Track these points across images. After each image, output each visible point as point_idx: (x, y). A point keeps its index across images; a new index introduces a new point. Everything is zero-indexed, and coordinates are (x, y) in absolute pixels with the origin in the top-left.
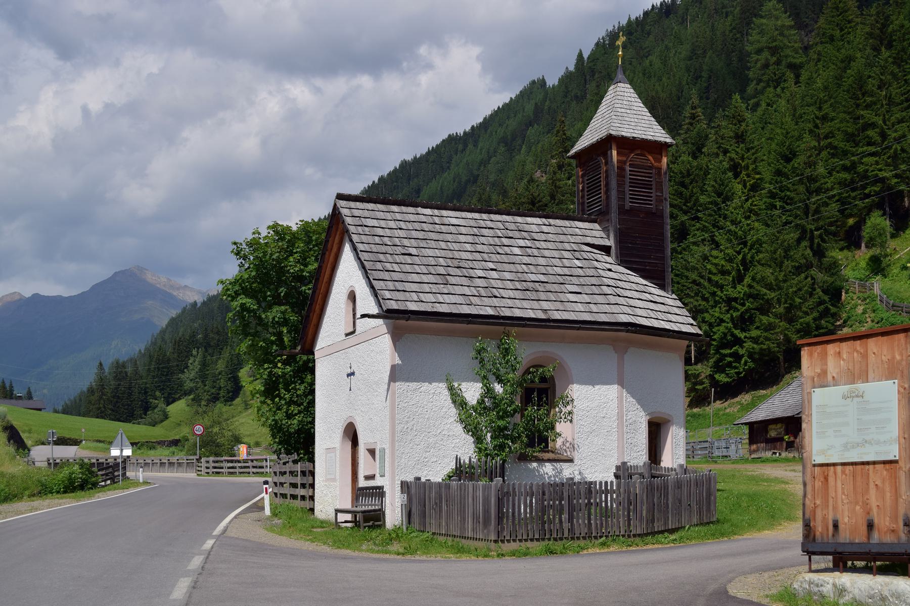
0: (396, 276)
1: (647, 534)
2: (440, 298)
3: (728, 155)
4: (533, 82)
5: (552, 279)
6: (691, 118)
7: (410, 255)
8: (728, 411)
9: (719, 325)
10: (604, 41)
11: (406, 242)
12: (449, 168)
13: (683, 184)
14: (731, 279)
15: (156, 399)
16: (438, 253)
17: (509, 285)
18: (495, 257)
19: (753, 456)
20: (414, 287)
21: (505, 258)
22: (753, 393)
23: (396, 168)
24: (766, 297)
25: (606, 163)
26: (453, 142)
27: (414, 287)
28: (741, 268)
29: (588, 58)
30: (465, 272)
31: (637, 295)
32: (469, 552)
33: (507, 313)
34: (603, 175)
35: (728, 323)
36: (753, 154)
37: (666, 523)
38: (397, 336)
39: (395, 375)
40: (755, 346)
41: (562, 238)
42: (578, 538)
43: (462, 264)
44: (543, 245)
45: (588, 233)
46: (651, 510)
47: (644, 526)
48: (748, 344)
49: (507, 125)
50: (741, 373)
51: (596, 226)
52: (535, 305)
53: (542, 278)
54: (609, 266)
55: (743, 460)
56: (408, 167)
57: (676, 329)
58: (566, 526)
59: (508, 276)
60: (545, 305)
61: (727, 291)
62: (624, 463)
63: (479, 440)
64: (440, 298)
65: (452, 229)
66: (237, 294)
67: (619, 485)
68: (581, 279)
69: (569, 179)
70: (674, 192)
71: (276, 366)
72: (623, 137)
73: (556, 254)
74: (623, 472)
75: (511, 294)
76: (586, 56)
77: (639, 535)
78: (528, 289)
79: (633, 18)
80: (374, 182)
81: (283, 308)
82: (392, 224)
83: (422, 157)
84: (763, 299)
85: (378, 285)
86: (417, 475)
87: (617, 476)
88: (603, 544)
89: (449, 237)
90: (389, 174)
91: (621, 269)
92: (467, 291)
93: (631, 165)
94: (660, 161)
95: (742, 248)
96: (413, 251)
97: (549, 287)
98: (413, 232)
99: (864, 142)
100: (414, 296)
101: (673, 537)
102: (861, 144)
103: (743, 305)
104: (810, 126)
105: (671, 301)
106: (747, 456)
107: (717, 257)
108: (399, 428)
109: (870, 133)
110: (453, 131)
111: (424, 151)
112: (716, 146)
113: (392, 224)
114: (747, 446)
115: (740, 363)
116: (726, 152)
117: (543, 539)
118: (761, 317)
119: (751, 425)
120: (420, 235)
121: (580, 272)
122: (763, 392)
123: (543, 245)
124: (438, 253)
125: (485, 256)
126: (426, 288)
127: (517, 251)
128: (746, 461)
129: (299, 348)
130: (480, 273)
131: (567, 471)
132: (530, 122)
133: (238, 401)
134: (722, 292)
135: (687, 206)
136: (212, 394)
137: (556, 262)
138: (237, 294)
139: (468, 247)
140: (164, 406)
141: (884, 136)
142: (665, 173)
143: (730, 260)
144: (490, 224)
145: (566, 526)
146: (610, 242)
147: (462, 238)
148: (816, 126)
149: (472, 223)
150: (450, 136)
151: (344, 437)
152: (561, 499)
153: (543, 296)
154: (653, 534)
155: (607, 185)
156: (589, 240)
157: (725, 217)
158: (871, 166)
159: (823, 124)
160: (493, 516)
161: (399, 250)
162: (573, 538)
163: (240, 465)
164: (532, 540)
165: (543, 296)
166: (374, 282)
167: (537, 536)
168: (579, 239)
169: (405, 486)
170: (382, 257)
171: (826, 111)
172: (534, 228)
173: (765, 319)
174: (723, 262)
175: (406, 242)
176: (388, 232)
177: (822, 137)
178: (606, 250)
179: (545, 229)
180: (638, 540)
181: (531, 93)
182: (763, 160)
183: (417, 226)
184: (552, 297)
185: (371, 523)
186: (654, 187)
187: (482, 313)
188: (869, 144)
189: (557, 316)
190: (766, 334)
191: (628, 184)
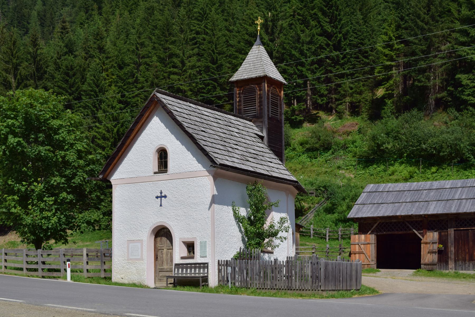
6: (62, 29)
13: (67, 74)
36: (110, 62)
38: (216, 177)
39: (214, 200)
70: (62, 79)
72: (271, 78)
99: (171, 65)
102: (169, 66)
104: (134, 47)
108: (216, 230)
109: (175, 60)
135: (71, 90)
141: (183, 63)
146: (264, 134)
148: (137, 49)
151: (151, 234)
158: (176, 81)
159: (141, 48)
171: (144, 40)
174: (104, 132)
177: (141, 56)
188: (174, 67)
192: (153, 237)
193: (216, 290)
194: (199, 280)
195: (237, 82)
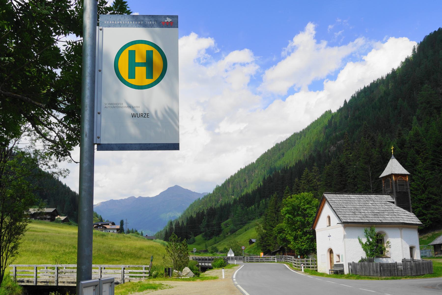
0: (343, 213)
1: (416, 275)
2: (355, 218)
3: (415, 148)
4: (327, 111)
5: (381, 212)
7: (345, 207)
8: (423, 239)
9: (416, 209)
10: (355, 95)
11: (343, 204)
12: (295, 145)
14: (420, 192)
15: (190, 235)
16: (351, 206)
17: (370, 214)
18: (365, 207)
19: (436, 256)
20: (348, 216)
21: (368, 207)
22: (432, 232)
23: (274, 146)
24: (434, 199)
25: (391, 180)
26: (296, 135)
27: (348, 216)
28: (424, 188)
29: (349, 102)
30: (359, 211)
31: (403, 214)
32: (373, 279)
33: (371, 221)
34: (391, 184)
35: (420, 208)
36: (425, 147)
37: (420, 273)
38: (345, 227)
40: (432, 216)
41: (381, 200)
42: (399, 276)
43: (358, 209)
44: (377, 202)
45: (388, 198)
46: (417, 271)
47: (415, 273)
48: (429, 216)
49: (317, 128)
50: (427, 225)
51: (389, 196)
52: (378, 219)
53: (378, 211)
54: (394, 207)
55: (431, 257)
56: (279, 146)
57: (415, 223)
58: (396, 273)
59: (369, 211)
60: (381, 219)
61: (419, 197)
62: (405, 259)
63: (367, 252)
64: (355, 218)
65: (353, 200)
66: (286, 214)
67: (403, 263)
68: (388, 211)
69: (350, 154)
71: (297, 232)
73: (380, 205)
74: (404, 261)
75: (371, 216)
76: (348, 101)
77: (414, 276)
78: (375, 215)
79: (366, 86)
80: (266, 152)
81: (300, 217)
82: (338, 199)
83: (284, 142)
84: (433, 199)
85: (339, 216)
86: (353, 261)
87: (402, 262)
88: (406, 278)
89: (353, 202)
90: (272, 149)
91: (398, 207)
92: (360, 216)
93: (398, 181)
94: (406, 179)
95: (423, 182)
96: (345, 206)
97: (380, 214)
98: (344, 201)
100: (348, 218)
101: (423, 276)
103: (426, 201)
105: (412, 215)
106: (434, 256)
107: (414, 185)
110: (296, 132)
111: (285, 139)
112: (409, 144)
113: (338, 199)
114: (434, 253)
115: (426, 222)
116: (413, 146)
117: (391, 276)
118: (433, 206)
119: (435, 246)
120: (345, 202)
121: (387, 209)
122: (436, 232)
123: (377, 202)
124: (351, 206)
125: (363, 206)
126: (351, 216)
127: (370, 205)
128: (434, 258)
129: (311, 229)
130: (363, 211)
131: (390, 261)
132: (327, 127)
133: (221, 235)
134: (417, 197)
136: (211, 232)
137: (381, 207)
138: (286, 214)
139: (358, 204)
140: (194, 237)
142: (408, 182)
143: (419, 185)
144: (362, 198)
145: (396, 273)
146: (394, 200)
147: (356, 202)
149: (358, 198)
150: (294, 133)
151: (328, 252)
152: (395, 267)
153: (379, 216)
154: (418, 275)
155: (392, 186)
156: (388, 200)
157: (416, 171)
160: (379, 270)
161: (342, 206)
162: (398, 276)
163: (260, 259)
164: (388, 276)
165: (379, 216)
166: (338, 215)
167: (389, 275)
168: (386, 200)
169: (349, 264)
170: (338, 208)
172: (373, 198)
173: (435, 207)
175: (343, 204)
176: (338, 202)
178: (393, 202)
179: (376, 198)
180: (414, 277)
181: (326, 115)
182: (428, 149)
183: (344, 199)
184: (382, 216)
185: (341, 273)
186: (405, 185)
187: (365, 221)
189: (384, 221)
190: (435, 212)
191: (398, 185)
192: (329, 253)
193: (348, 277)
194: (338, 272)
195: (382, 177)
